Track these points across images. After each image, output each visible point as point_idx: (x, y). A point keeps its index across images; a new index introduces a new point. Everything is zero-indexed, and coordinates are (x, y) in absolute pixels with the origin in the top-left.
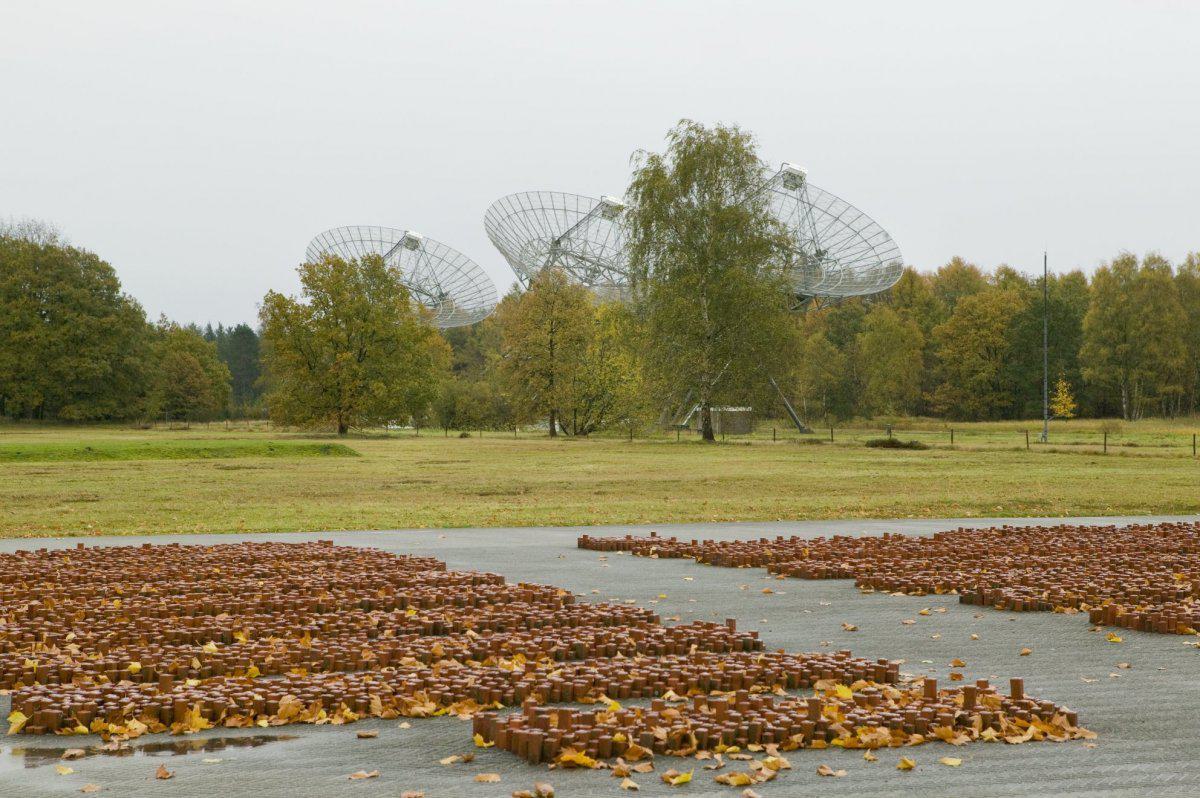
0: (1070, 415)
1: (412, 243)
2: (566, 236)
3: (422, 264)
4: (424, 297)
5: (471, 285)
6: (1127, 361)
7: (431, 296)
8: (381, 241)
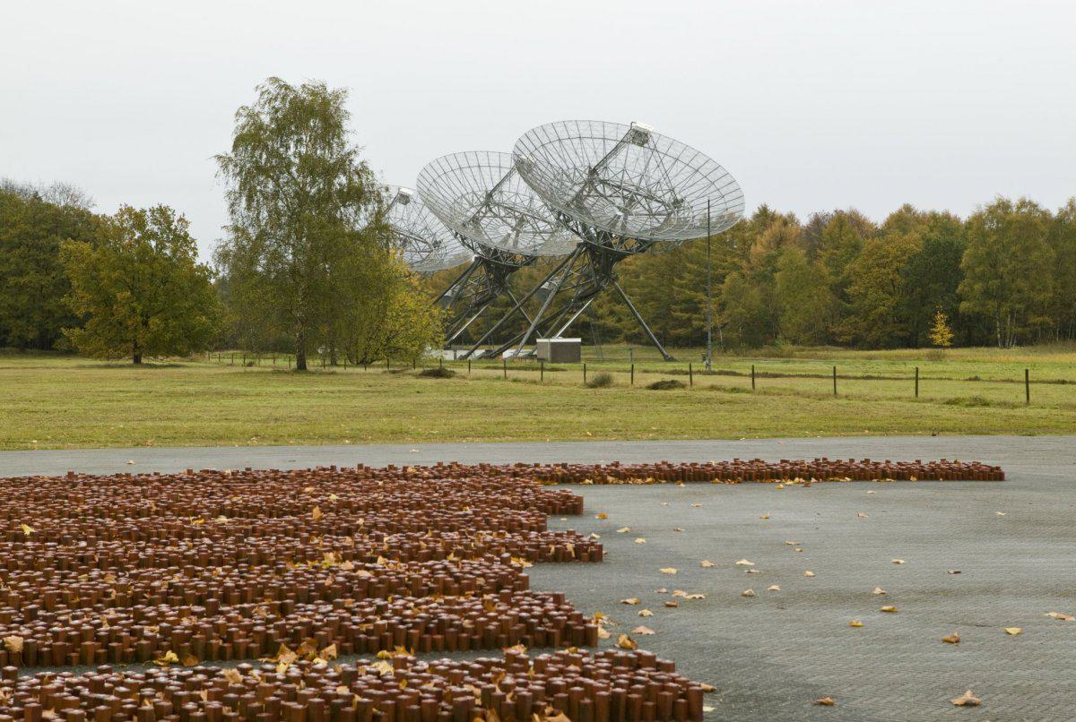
0: (947, 344)
1: (640, 137)
2: (604, 163)
3: (653, 164)
4: (654, 205)
5: (712, 188)
6: (999, 295)
7: (663, 203)
8: (604, 139)
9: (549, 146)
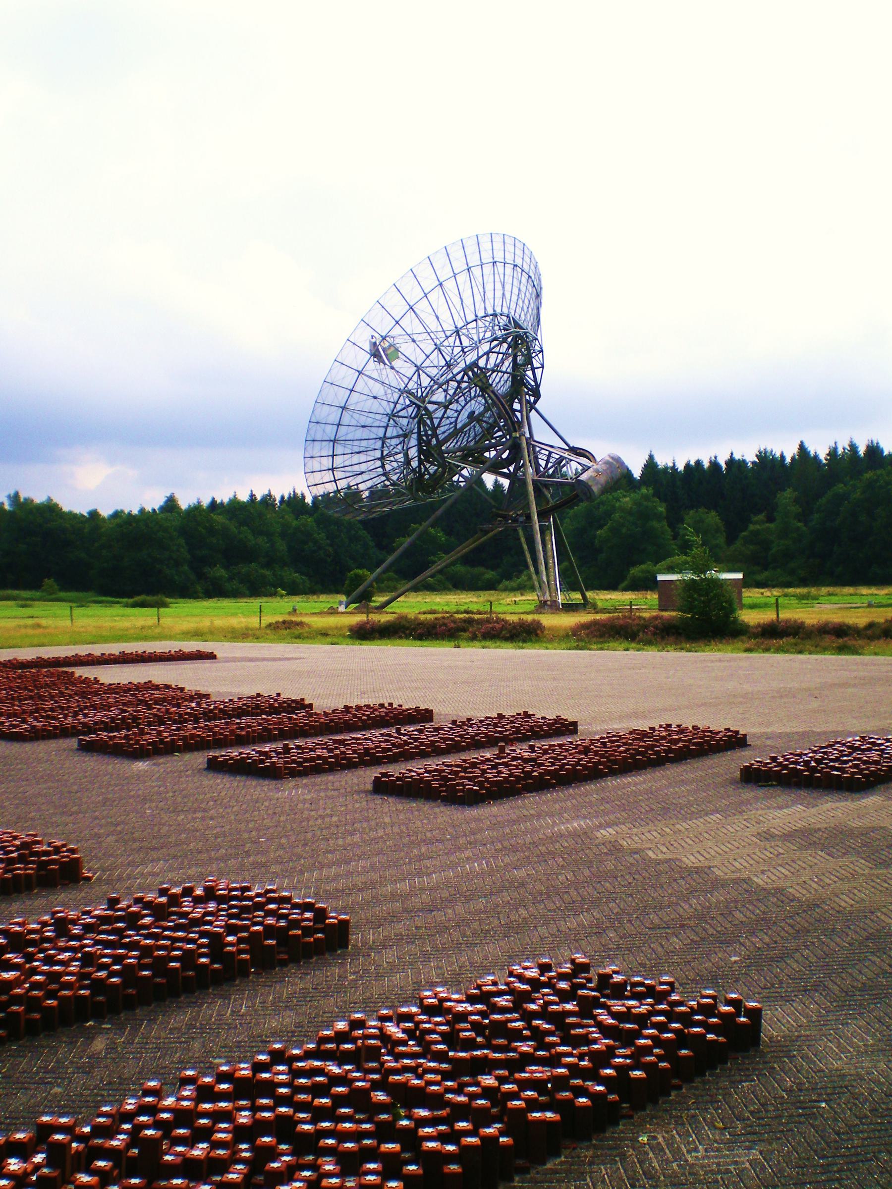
9: (338, 461)
